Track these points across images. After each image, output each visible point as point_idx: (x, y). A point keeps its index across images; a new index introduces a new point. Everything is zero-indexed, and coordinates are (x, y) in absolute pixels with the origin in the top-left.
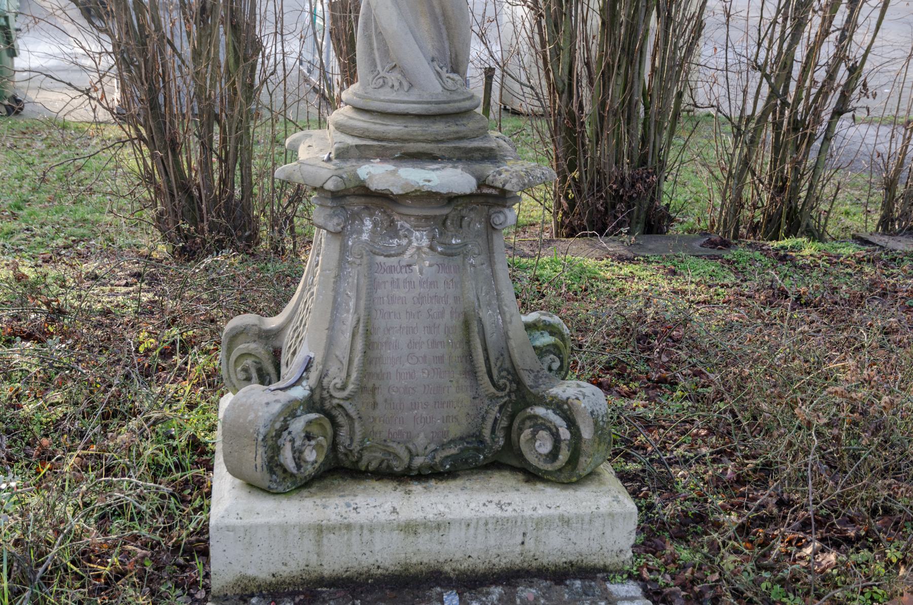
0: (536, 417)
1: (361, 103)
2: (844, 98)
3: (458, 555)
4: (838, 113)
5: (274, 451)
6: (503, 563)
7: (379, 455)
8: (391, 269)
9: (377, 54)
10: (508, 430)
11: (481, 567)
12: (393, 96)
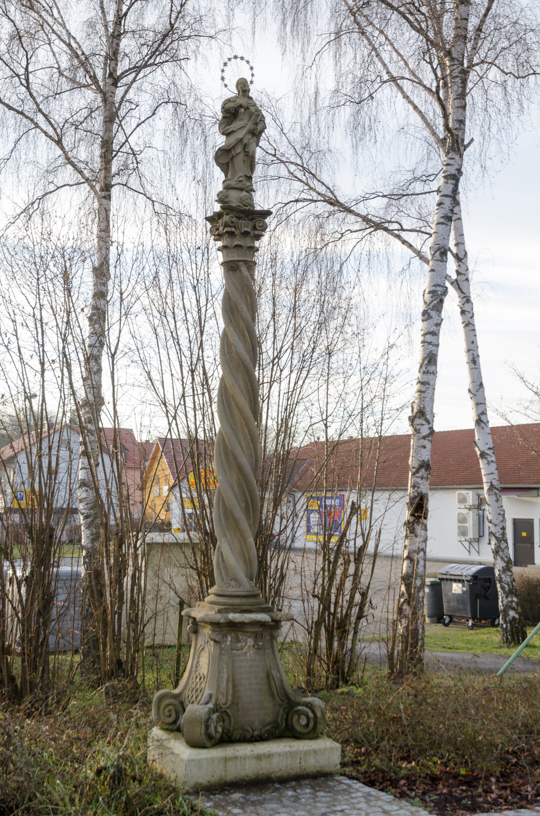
0: (298, 711)
1: (219, 593)
2: (361, 610)
3: (277, 770)
4: (360, 616)
5: (207, 727)
6: (293, 772)
7: (240, 732)
8: (239, 655)
9: (224, 575)
10: (286, 719)
11: (285, 775)
12: (234, 590)
